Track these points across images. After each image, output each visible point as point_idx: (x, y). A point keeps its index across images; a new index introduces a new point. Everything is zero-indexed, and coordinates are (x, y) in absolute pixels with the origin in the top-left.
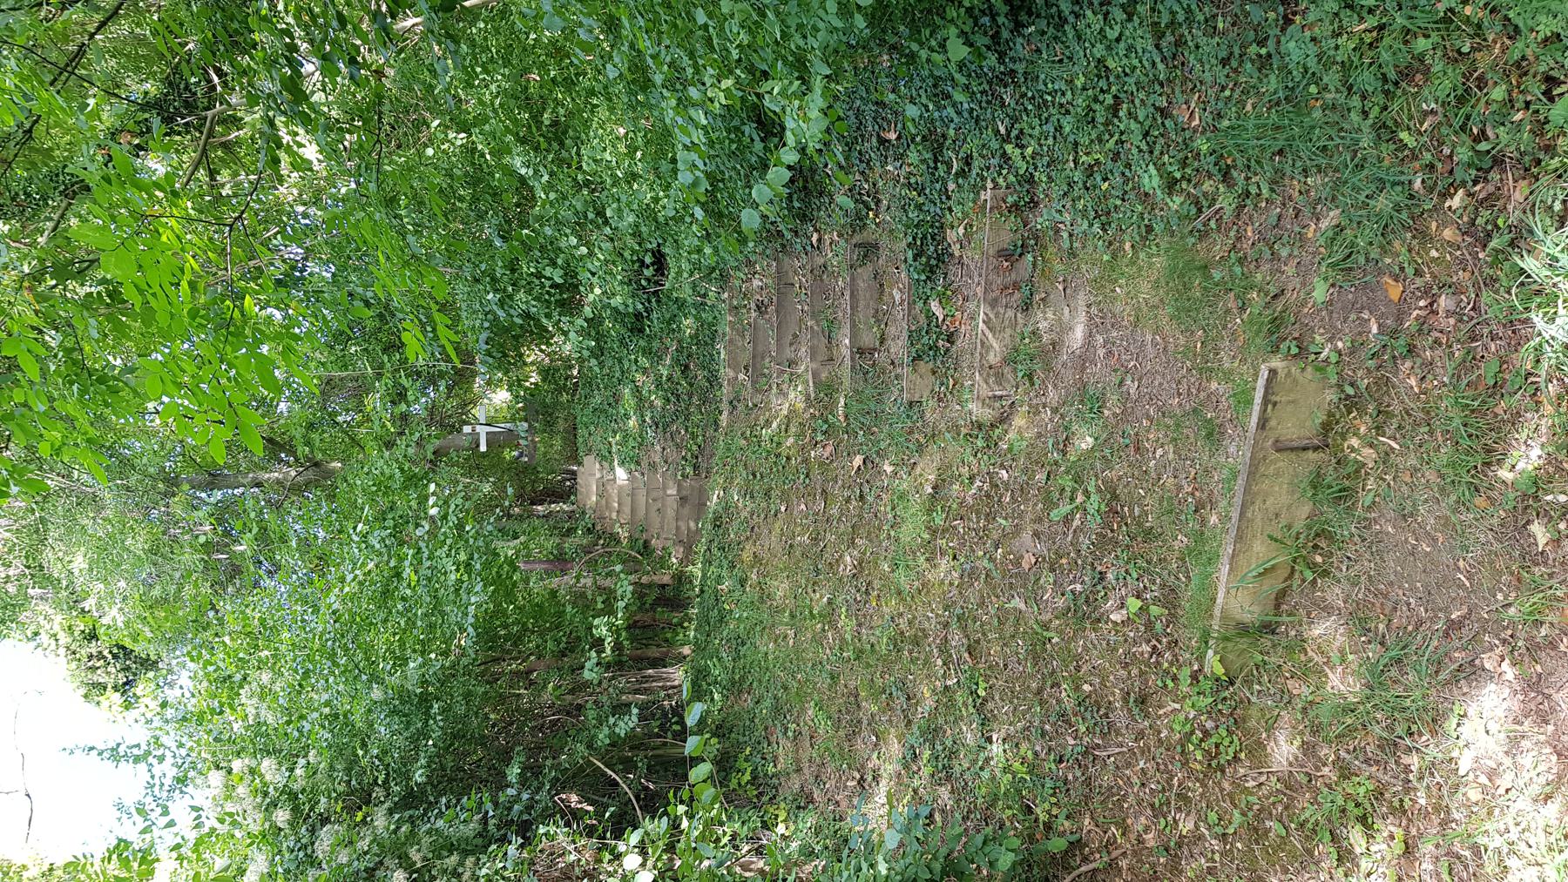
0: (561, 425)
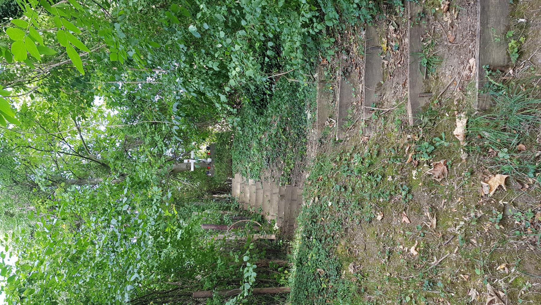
0: (225, 159)
